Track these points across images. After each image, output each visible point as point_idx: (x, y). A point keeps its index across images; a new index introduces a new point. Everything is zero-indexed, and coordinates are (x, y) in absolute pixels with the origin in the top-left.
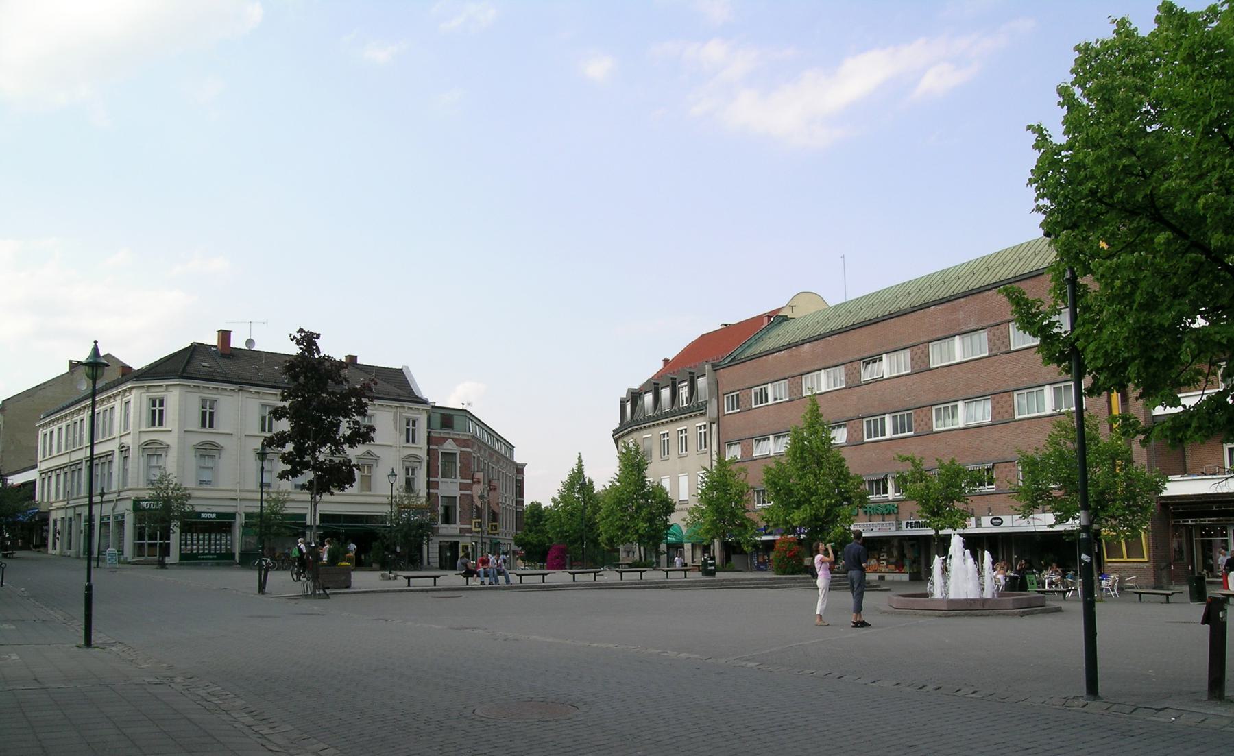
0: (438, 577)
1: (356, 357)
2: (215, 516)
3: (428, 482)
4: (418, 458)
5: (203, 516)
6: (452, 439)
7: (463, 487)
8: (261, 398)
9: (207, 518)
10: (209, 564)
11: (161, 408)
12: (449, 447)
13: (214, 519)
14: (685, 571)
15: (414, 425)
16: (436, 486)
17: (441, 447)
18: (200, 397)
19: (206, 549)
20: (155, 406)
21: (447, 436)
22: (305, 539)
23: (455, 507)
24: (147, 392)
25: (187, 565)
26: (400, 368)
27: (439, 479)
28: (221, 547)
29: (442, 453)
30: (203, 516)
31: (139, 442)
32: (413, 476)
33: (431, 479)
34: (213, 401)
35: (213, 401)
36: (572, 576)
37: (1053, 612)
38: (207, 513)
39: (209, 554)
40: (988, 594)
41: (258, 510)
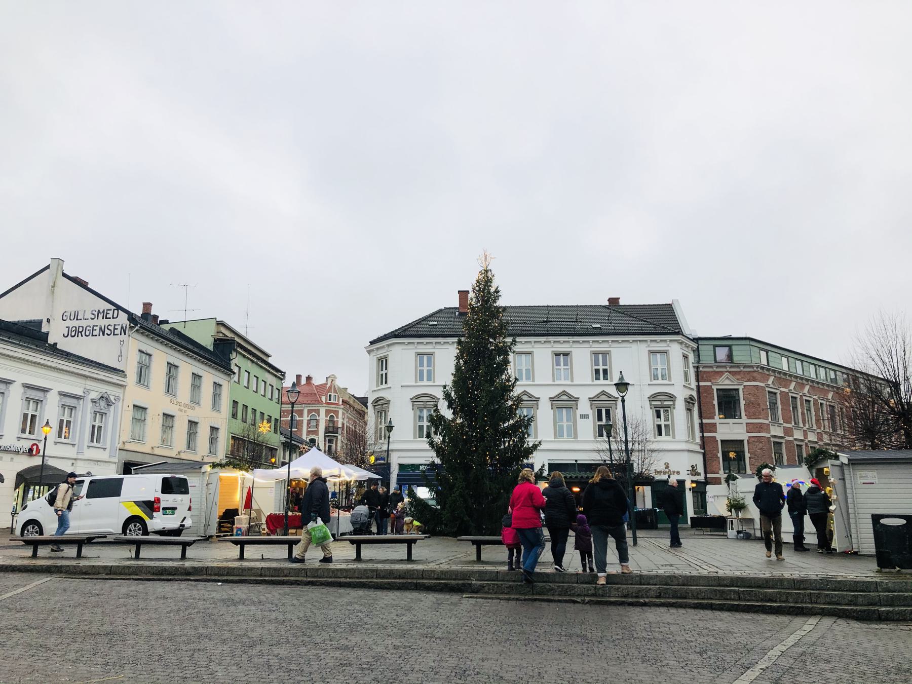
0: (473, 562)
1: (618, 299)
3: (701, 425)
4: (672, 398)
6: (730, 372)
7: (750, 428)
8: (552, 347)
14: (138, 544)
15: (421, 372)
16: (713, 428)
18: (553, 351)
20: (560, 365)
23: (744, 452)
26: (670, 303)
29: (717, 389)
33: (705, 421)
34: (605, 354)
35: (605, 354)
36: (475, 546)
37: (75, 573)
40: (670, 526)
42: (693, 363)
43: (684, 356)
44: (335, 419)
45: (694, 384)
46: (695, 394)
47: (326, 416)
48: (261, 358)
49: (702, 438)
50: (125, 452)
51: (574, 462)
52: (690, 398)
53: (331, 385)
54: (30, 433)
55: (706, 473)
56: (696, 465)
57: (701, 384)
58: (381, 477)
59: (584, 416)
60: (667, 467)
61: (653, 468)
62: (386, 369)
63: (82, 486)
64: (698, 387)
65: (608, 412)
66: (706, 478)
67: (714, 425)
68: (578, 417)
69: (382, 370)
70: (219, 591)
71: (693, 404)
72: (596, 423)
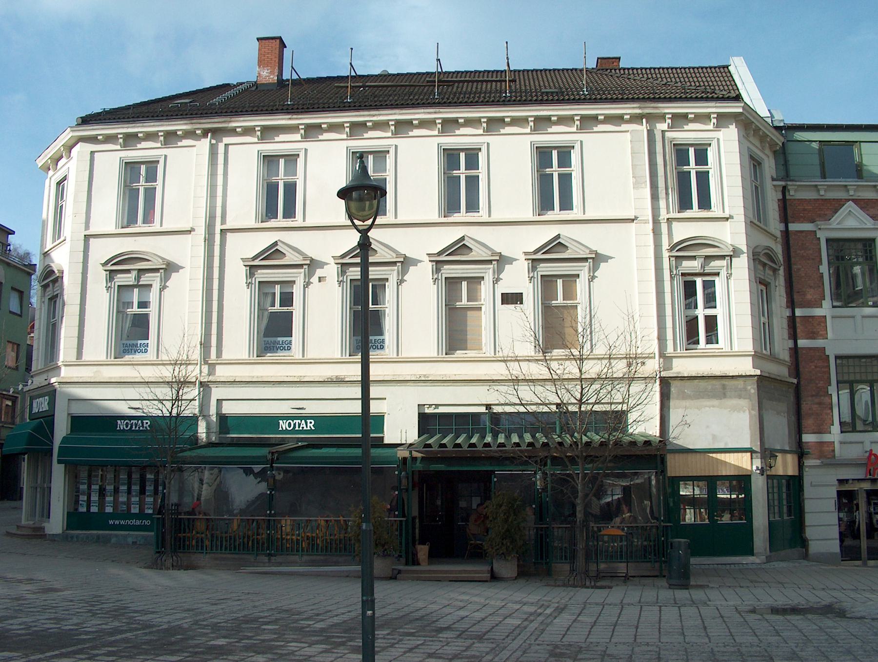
2: (311, 425)
3: (792, 321)
5: (283, 425)
9: (294, 431)
10: (113, 540)
11: (472, 172)
12: (851, 223)
13: (310, 431)
16: (816, 327)
17: (822, 224)
19: (83, 494)
21: (840, 195)
22: (595, 516)
24: (535, 130)
25: (318, 575)
27: (825, 310)
28: (129, 499)
30: (283, 425)
31: (44, 264)
32: (285, 309)
38: (293, 418)
39: (141, 515)
41: (356, 408)
42: (773, 179)
43: (752, 157)
45: (775, 226)
46: (778, 249)
50: (126, 399)
51: (483, 409)
52: (767, 255)
54: (446, 354)
57: (793, 227)
58: (178, 455)
59: (512, 299)
64: (786, 233)
65: (709, 286)
71: (775, 271)
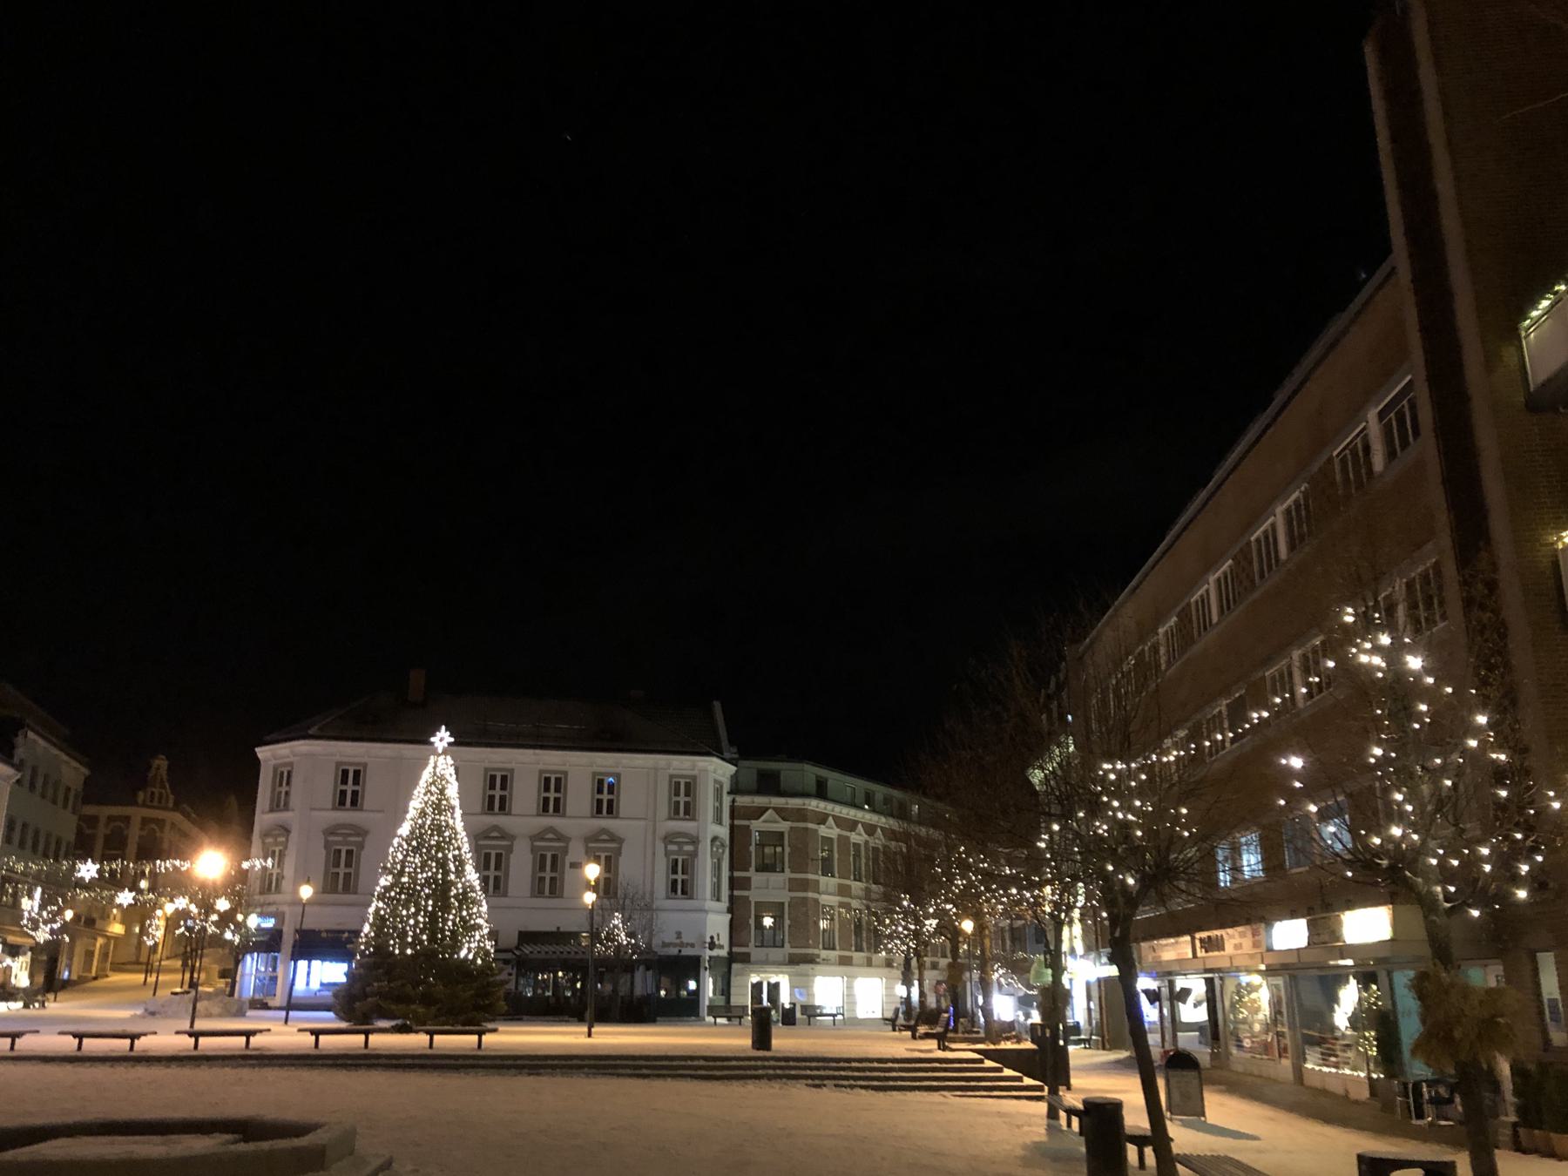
3: (731, 879)
16: (745, 884)
44: (158, 834)
47: (142, 829)
48: (606, 1060)
49: (731, 898)
53: (156, 775)
55: (731, 944)
56: (718, 935)
60: (679, 935)
61: (656, 942)
62: (288, 783)
63: (1098, 1049)
66: (730, 953)
67: (749, 879)
68: (567, 865)
69: (281, 785)
70: (228, 1073)
72: (604, 852)
